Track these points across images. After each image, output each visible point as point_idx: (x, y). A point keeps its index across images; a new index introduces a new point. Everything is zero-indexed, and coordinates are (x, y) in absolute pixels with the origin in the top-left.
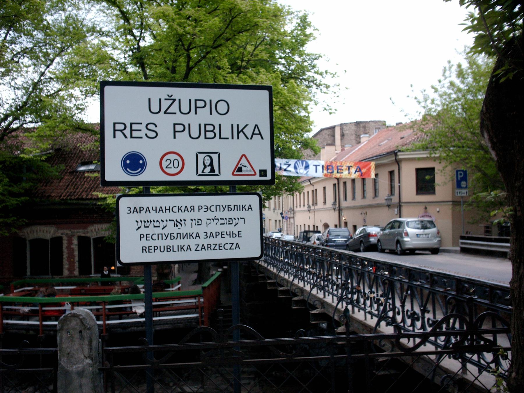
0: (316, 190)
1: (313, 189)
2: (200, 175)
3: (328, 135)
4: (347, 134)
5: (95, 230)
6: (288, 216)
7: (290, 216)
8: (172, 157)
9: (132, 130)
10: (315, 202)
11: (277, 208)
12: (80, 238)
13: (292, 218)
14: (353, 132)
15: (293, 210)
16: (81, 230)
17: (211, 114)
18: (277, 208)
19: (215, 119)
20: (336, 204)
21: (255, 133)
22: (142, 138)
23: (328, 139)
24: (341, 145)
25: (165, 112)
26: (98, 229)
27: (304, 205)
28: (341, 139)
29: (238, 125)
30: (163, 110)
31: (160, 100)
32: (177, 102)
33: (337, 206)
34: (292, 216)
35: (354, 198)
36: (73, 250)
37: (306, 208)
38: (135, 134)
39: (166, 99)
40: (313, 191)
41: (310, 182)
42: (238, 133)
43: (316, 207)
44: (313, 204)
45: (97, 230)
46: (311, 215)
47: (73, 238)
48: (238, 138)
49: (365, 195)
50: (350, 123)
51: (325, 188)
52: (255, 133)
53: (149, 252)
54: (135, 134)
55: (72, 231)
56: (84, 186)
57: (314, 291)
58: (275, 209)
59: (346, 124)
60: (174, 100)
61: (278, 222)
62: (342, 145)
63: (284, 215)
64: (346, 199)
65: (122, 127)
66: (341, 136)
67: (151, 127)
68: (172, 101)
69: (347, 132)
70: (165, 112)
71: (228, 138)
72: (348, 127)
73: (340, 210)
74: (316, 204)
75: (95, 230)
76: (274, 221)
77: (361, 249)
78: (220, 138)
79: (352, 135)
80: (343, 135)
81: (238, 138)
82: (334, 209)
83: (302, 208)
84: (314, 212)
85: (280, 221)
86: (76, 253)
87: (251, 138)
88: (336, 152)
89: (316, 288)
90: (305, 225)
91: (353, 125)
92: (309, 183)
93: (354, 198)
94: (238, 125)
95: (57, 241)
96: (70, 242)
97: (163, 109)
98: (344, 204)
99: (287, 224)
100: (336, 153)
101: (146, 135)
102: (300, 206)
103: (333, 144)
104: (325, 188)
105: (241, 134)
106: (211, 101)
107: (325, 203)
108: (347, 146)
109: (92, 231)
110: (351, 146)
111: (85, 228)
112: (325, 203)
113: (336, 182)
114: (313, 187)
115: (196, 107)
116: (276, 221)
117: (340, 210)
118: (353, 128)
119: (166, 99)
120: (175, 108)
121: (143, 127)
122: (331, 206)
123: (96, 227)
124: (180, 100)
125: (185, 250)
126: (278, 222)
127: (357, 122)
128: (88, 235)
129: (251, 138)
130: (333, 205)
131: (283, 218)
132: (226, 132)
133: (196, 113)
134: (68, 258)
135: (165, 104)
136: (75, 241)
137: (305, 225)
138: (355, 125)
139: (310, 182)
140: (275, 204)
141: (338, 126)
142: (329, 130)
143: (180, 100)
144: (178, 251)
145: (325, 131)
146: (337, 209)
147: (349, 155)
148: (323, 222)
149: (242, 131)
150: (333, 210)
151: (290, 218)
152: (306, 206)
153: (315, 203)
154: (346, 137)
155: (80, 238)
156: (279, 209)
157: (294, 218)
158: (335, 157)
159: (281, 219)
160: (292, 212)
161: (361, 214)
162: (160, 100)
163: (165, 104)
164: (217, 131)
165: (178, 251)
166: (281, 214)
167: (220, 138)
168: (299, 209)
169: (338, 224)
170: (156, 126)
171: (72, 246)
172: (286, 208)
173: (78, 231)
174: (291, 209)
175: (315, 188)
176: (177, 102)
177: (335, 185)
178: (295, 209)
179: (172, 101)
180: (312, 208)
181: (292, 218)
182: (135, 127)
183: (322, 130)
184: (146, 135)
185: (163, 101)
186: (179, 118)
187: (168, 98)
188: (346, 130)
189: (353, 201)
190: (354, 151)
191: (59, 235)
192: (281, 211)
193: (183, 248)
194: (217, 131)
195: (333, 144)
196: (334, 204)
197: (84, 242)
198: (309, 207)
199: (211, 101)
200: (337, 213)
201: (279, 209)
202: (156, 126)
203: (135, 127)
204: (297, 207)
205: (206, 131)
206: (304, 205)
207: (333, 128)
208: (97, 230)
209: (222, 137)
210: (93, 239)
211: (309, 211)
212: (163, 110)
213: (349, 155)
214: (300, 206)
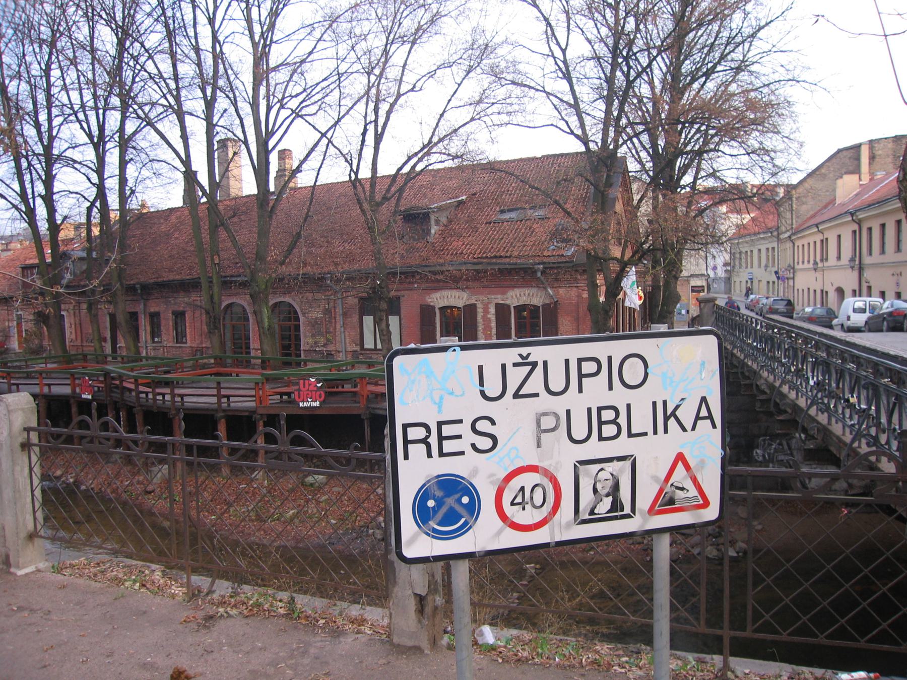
0: (827, 239)
1: (822, 238)
2: (584, 522)
3: (850, 158)
4: (880, 155)
5: (516, 296)
6: (786, 276)
7: (788, 276)
8: (528, 480)
9: (441, 439)
10: (824, 257)
11: (770, 264)
12: (499, 307)
13: (791, 278)
14: (890, 152)
15: (793, 268)
16: (499, 296)
17: (611, 388)
18: (770, 264)
19: (620, 397)
20: (855, 261)
21: (701, 415)
22: (462, 453)
23: (849, 164)
24: (869, 172)
25: (516, 395)
26: (520, 295)
27: (809, 262)
28: (870, 164)
29: (665, 403)
30: (511, 390)
31: (504, 366)
32: (540, 369)
33: (857, 262)
34: (792, 275)
35: (883, 251)
36: (490, 320)
37: (811, 265)
38: (448, 446)
39: (515, 365)
40: (822, 241)
41: (818, 228)
42: (666, 419)
43: (826, 264)
44: (822, 260)
45: (518, 295)
46: (819, 275)
47: (489, 306)
48: (666, 431)
49: (900, 248)
50: (886, 138)
51: (839, 236)
52: (701, 415)
53: (442, 454)
54: (448, 446)
55: (489, 296)
56: (503, 241)
57: (813, 411)
58: (766, 266)
59: (879, 140)
60: (534, 365)
61: (771, 283)
62: (872, 171)
63: (781, 273)
64: (870, 253)
65: (420, 433)
66: (869, 159)
67: (482, 426)
68: (530, 367)
69: (880, 152)
70: (516, 395)
71: (645, 434)
72: (882, 145)
73: (861, 269)
74: (827, 259)
75: (516, 296)
76: (766, 283)
77: (884, 328)
78: (630, 435)
79: (888, 156)
80: (872, 158)
81: (666, 431)
82: (852, 268)
83: (806, 265)
84: (823, 271)
85: (774, 282)
86: (493, 324)
87: (693, 428)
88: (861, 183)
89: (815, 407)
90: (809, 289)
91: (890, 141)
92: (816, 230)
93: (883, 251)
94: (665, 403)
95: (471, 309)
96: (486, 311)
97: (511, 389)
98: (867, 260)
99: (784, 288)
100: (861, 185)
101: (473, 446)
102: (803, 262)
103: (857, 170)
104: (839, 236)
105: (672, 422)
106: (610, 358)
107: (839, 258)
108: (878, 173)
109: (512, 297)
110: (884, 173)
111: (504, 293)
112: (839, 258)
113: (856, 227)
114: (821, 235)
115: (581, 376)
116: (768, 282)
117: (861, 269)
118: (890, 145)
119: (515, 365)
120: (535, 383)
121: (464, 429)
122: (848, 263)
123: (517, 291)
124: (545, 363)
125: (688, 424)
126: (771, 283)
127: (896, 137)
128: (508, 302)
129: (693, 428)
130: (850, 261)
131: (778, 278)
132: (642, 421)
133: (580, 391)
134: (484, 329)
135: (515, 376)
136: (492, 310)
137: (809, 289)
138: (893, 142)
139: (818, 228)
140: (768, 259)
141: (865, 144)
142: (852, 151)
143: (545, 363)
144: (655, 432)
145: (845, 153)
146: (857, 267)
147: (878, 188)
148: (836, 286)
149: (673, 414)
150: (851, 269)
151: (788, 279)
152: (812, 262)
153: (824, 259)
154: (877, 160)
155: (499, 307)
156: (773, 266)
157: (793, 278)
158: (858, 190)
159: (776, 280)
160: (792, 271)
161: (893, 275)
162: (504, 366)
163: (515, 376)
164: (623, 420)
165: (655, 432)
166: (776, 273)
167: (630, 435)
168: (801, 266)
169: (857, 289)
170: (493, 422)
171: (489, 316)
172: (783, 265)
173: (496, 296)
174: (789, 266)
175: (825, 237)
176: (540, 369)
177: (854, 232)
178: (796, 267)
179: (530, 367)
180: (820, 265)
181: (791, 278)
182: (447, 430)
183: (839, 151)
184: (473, 446)
185: (509, 368)
186: (545, 402)
187: (520, 360)
188: (878, 150)
189: (882, 256)
190: (887, 181)
191: (473, 302)
192: (776, 269)
193: (673, 414)
194: (623, 420)
195: (857, 170)
196: (852, 260)
197: (502, 311)
198: (815, 263)
199: (610, 358)
200: (856, 274)
201: (773, 266)
202: (493, 422)
203: (447, 430)
204: (798, 263)
205: (601, 423)
206: (809, 262)
207: (857, 148)
208: (518, 295)
209: (633, 432)
210: (514, 307)
211: (815, 269)
212: (511, 389)
213: (878, 188)
214: (803, 262)
